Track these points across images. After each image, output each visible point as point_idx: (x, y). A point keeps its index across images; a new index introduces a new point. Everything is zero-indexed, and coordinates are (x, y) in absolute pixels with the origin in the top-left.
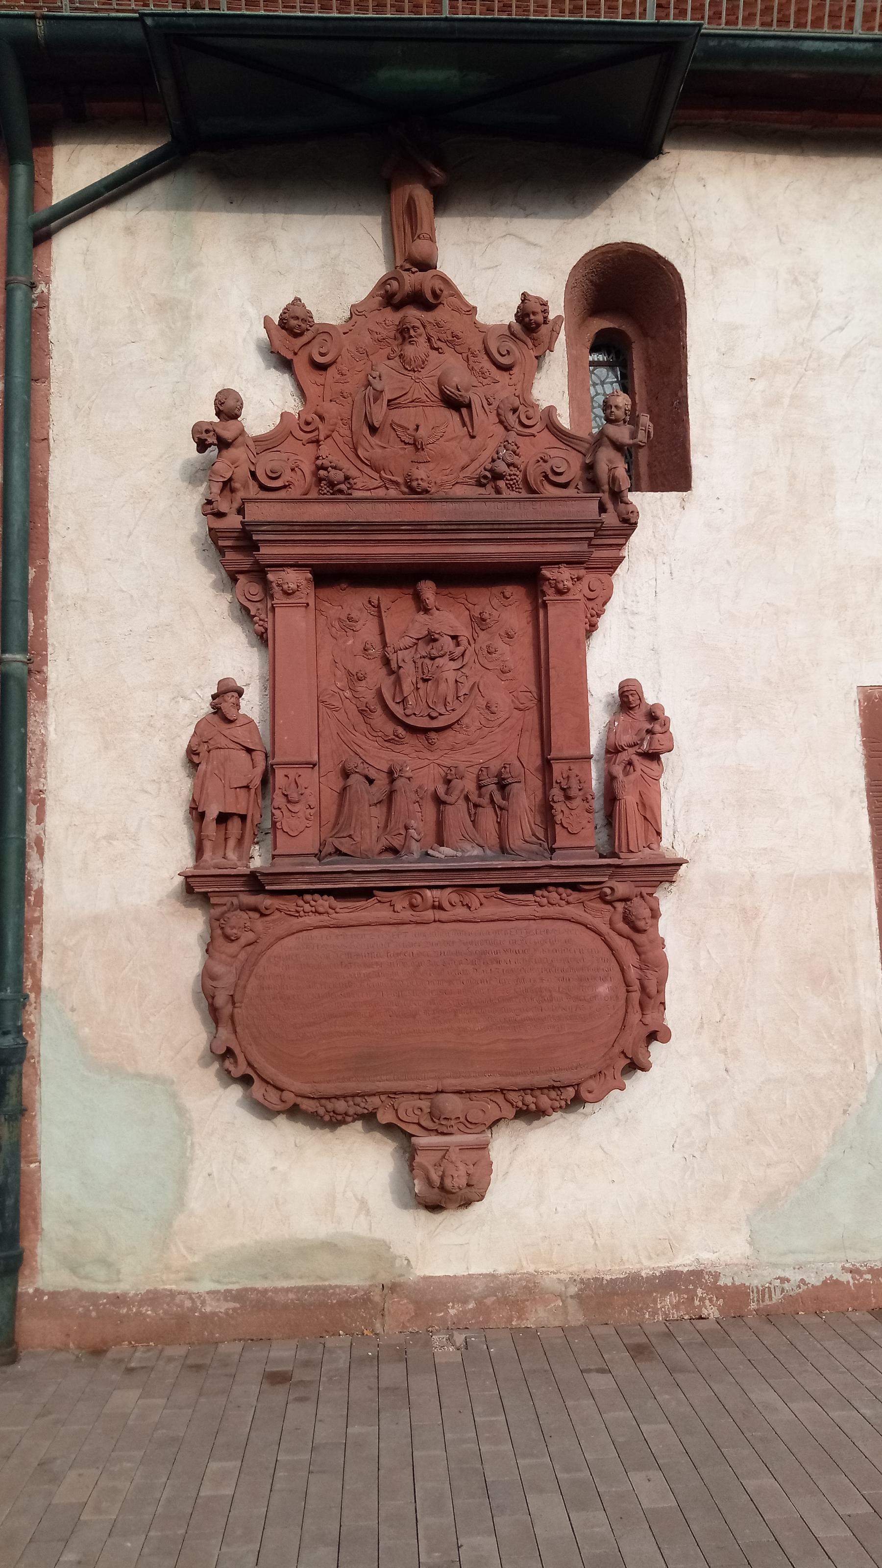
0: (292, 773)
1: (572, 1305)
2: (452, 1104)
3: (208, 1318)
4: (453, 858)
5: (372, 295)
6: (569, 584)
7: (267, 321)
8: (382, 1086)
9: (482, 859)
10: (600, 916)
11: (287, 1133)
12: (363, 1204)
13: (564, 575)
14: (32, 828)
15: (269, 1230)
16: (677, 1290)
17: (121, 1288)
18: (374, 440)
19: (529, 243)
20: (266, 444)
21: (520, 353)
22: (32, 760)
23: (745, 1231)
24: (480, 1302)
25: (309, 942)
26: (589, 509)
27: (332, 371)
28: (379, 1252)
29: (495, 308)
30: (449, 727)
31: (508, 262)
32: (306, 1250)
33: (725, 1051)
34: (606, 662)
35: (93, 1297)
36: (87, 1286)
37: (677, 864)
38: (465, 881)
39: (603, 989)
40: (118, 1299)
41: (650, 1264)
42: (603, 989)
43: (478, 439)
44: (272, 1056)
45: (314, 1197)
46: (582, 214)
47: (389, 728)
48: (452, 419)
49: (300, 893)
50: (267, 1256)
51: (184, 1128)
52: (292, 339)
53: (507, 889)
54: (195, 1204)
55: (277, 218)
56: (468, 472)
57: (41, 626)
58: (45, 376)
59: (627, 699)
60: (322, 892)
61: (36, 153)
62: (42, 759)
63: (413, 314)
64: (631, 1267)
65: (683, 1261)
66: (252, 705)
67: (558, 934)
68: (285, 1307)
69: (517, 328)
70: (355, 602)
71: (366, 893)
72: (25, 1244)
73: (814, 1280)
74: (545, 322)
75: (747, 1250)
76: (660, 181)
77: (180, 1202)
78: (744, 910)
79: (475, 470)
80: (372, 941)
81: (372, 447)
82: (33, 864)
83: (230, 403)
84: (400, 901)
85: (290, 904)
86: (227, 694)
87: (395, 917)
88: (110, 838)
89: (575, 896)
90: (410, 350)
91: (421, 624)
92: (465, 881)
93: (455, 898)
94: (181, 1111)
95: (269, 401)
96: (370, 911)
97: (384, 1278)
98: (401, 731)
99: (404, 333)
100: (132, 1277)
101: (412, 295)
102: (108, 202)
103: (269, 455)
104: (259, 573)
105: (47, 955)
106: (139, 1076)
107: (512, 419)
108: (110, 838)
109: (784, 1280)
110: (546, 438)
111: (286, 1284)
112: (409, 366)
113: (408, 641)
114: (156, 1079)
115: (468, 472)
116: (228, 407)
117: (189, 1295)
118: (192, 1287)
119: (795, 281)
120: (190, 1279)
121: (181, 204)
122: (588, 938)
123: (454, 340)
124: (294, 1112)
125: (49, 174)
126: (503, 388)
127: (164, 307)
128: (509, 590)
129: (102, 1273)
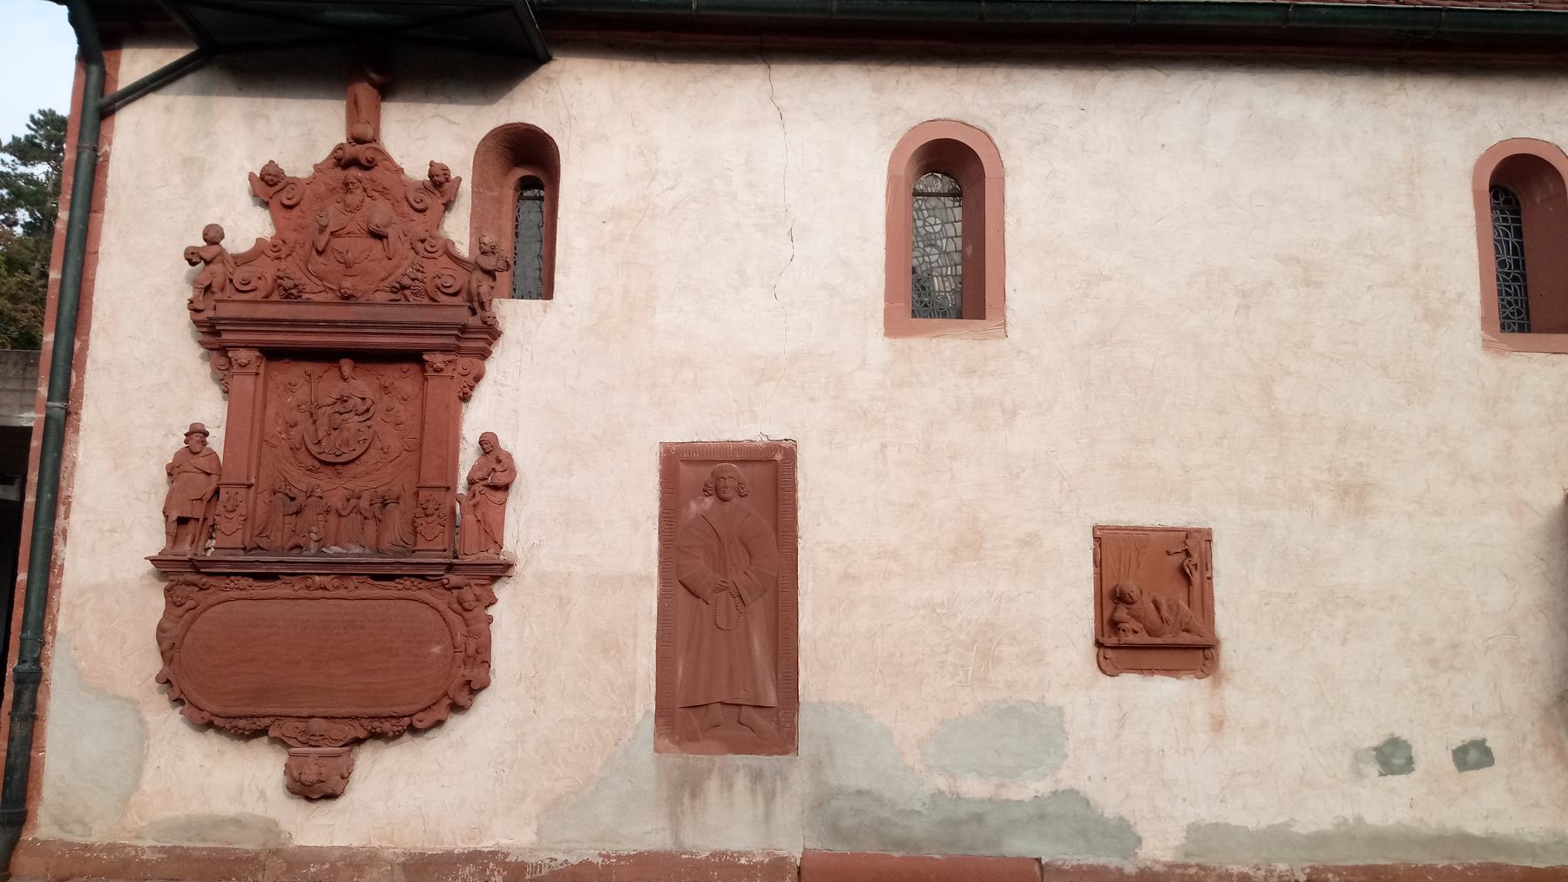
0: (232, 491)
1: (398, 869)
2: (317, 725)
3: (143, 863)
4: (340, 555)
5: (329, 158)
6: (441, 366)
7: (251, 176)
8: (271, 711)
9: (359, 555)
10: (442, 600)
11: (213, 742)
12: (262, 795)
13: (438, 359)
14: (60, 522)
15: (196, 808)
16: (476, 864)
17: (89, 841)
18: (321, 259)
19: (451, 122)
20: (241, 260)
21: (435, 202)
22: (64, 474)
23: (534, 827)
24: (333, 865)
25: (235, 608)
26: (464, 316)
27: (297, 210)
28: (271, 827)
29: (416, 171)
30: (352, 461)
31: (433, 137)
32: (219, 823)
33: (535, 698)
34: (476, 419)
35: (70, 845)
36: (68, 838)
37: (153, 560)
38: (343, 570)
39: (436, 650)
40: (86, 847)
41: (459, 843)
42: (436, 650)
43: (395, 261)
44: (212, 689)
45: (233, 785)
46: (491, 102)
47: (310, 462)
48: (377, 246)
49: (228, 575)
50: (193, 825)
51: (143, 735)
52: (270, 186)
53: (257, 577)
54: (147, 786)
55: (272, 102)
56: (386, 283)
57: (80, 382)
58: (101, 209)
59: (488, 445)
60: (244, 575)
61: (105, 54)
62: (72, 474)
63: (354, 173)
64: (447, 846)
65: (486, 844)
66: (216, 441)
67: (405, 610)
68: (197, 860)
69: (429, 185)
70: (295, 372)
71: (274, 577)
72: (30, 807)
73: (574, 860)
74: (447, 180)
75: (534, 838)
76: (549, 80)
77: (136, 785)
78: (560, 598)
79: (391, 281)
80: (278, 608)
81: (318, 263)
82: (58, 547)
83: (211, 234)
84: (299, 583)
85: (221, 582)
86: (197, 434)
87: (294, 595)
88: (112, 531)
89: (425, 583)
90: (350, 198)
91: (340, 388)
92: (343, 570)
93: (336, 582)
94: (142, 722)
95: (248, 228)
96: (279, 589)
97: (272, 845)
98: (317, 464)
99: (347, 186)
100: (99, 832)
101: (358, 159)
102: (155, 89)
103: (244, 268)
104: (223, 350)
105: (63, 610)
106: (117, 697)
107: (420, 246)
108: (112, 531)
109: (552, 860)
110: (445, 260)
111: (202, 845)
112: (351, 210)
113: (331, 401)
114: (127, 700)
115: (386, 283)
116: (213, 236)
117: (135, 848)
118: (139, 843)
119: (642, 153)
120: (138, 837)
121: (205, 91)
122: (430, 613)
123: (384, 192)
124: (219, 730)
125: (117, 69)
126: (419, 225)
127: (187, 162)
128: (405, 366)
129: (79, 830)
